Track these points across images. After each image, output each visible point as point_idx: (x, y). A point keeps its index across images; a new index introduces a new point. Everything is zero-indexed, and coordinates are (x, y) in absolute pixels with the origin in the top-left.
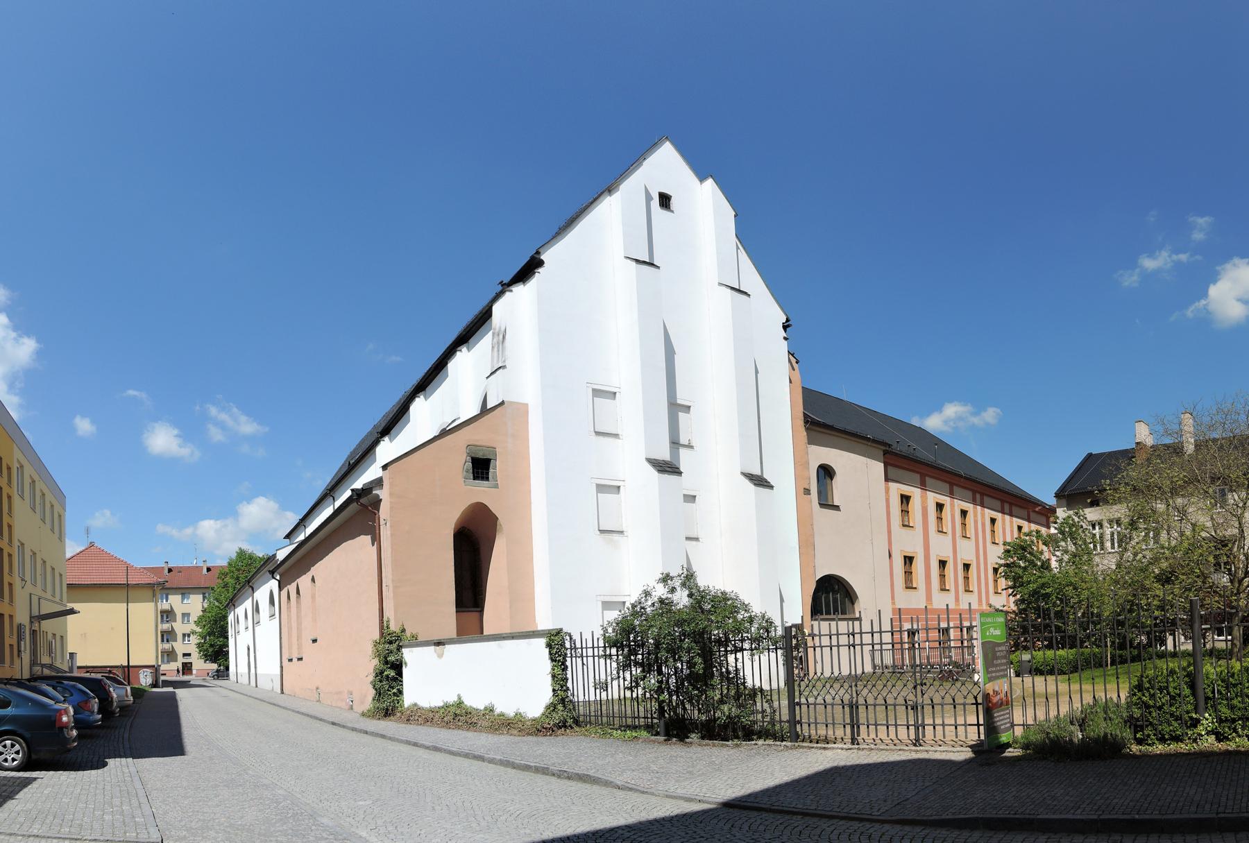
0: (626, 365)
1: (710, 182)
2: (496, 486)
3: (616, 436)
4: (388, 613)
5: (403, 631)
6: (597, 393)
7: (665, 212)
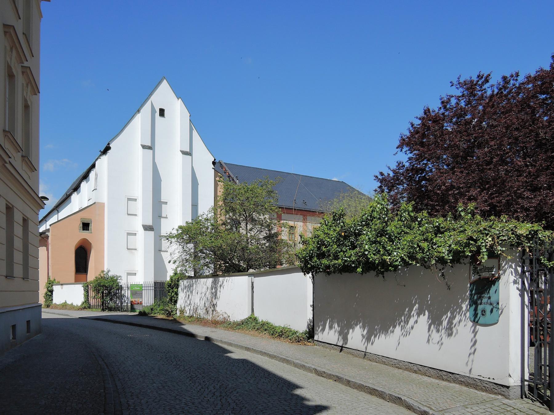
0: (139, 187)
1: (180, 99)
2: (91, 233)
3: (136, 215)
4: (50, 274)
5: (55, 280)
6: (129, 199)
7: (162, 118)
